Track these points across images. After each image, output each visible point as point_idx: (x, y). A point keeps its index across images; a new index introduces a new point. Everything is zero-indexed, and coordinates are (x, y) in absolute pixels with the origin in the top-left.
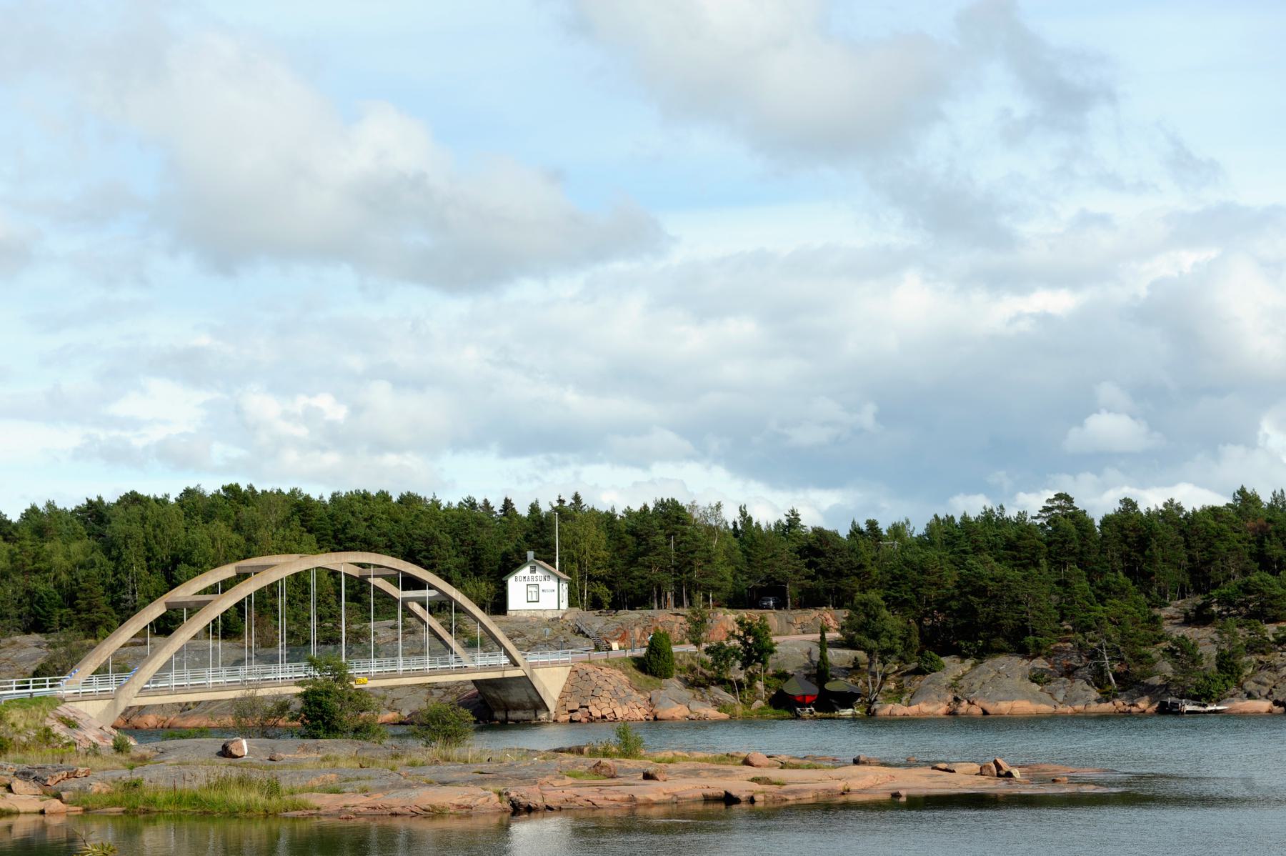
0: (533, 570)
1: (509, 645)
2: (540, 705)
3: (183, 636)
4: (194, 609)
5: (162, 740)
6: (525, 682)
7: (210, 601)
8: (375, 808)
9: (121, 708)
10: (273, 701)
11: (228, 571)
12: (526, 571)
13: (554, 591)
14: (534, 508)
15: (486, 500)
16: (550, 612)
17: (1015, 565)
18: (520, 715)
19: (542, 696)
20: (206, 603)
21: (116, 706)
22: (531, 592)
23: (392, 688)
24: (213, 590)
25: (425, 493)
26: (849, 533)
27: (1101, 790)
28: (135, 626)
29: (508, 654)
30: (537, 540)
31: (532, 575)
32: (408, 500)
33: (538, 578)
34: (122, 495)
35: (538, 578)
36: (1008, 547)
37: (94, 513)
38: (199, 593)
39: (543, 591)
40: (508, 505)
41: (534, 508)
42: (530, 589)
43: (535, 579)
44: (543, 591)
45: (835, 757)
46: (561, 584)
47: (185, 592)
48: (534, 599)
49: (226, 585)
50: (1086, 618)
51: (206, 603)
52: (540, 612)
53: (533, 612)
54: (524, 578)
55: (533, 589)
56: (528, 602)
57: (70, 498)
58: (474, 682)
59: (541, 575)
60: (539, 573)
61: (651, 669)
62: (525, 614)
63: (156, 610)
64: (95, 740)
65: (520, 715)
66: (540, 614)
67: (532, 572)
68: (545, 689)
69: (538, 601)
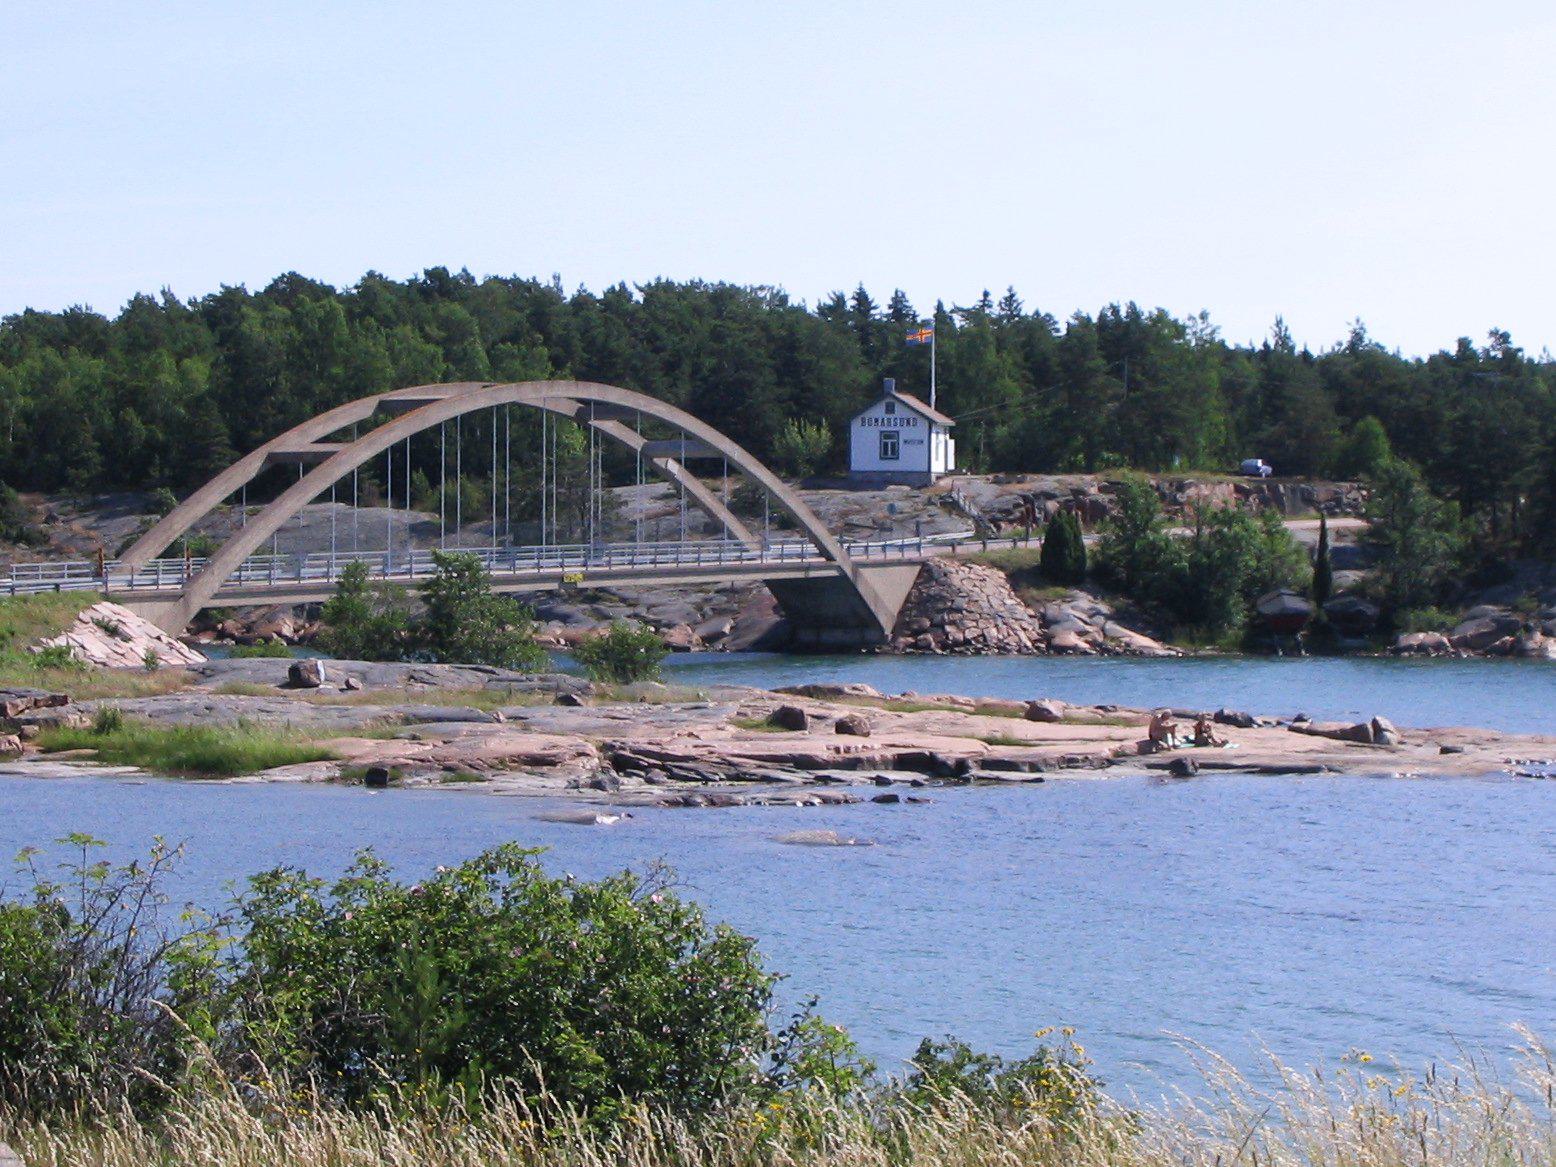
1: (818, 528)
2: (870, 620)
3: (293, 503)
4: (312, 462)
5: (225, 657)
6: (844, 586)
7: (334, 453)
8: (422, 761)
9: (195, 610)
11: (362, 409)
15: (464, 270)
18: (838, 636)
19: (872, 608)
20: (327, 455)
21: (187, 606)
23: (650, 589)
24: (343, 435)
25: (681, 278)
27: (996, 774)
28: (223, 488)
29: (815, 540)
31: (888, 416)
32: (661, 293)
36: (874, 342)
37: (226, 308)
38: (317, 442)
39: (905, 442)
40: (898, 303)
45: (563, 710)
46: (933, 436)
47: (296, 441)
49: (364, 428)
51: (327, 455)
54: (876, 420)
57: (194, 286)
58: (767, 583)
63: (251, 466)
65: (838, 636)
68: (876, 597)
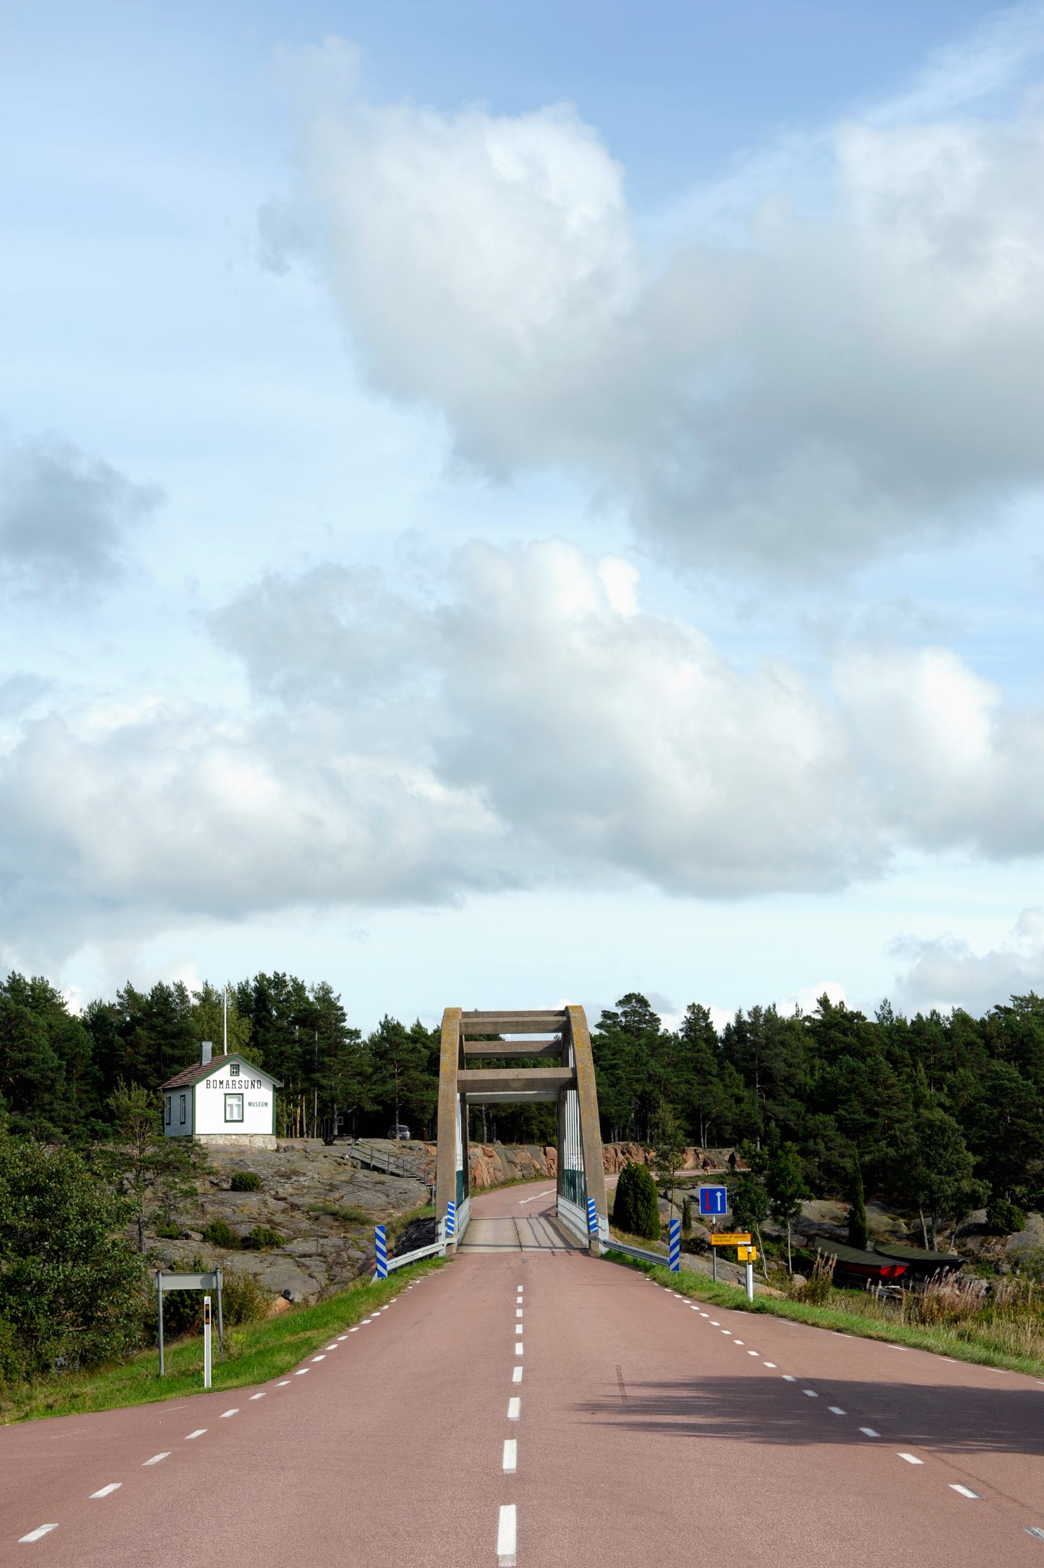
0: (235, 1070)
10: (199, 1261)
12: (224, 1073)
13: (266, 1104)
14: (698, 1018)
16: (260, 1138)
17: (415, 1080)
22: (231, 1106)
26: (733, 1024)
30: (161, 1026)
31: (234, 1078)
33: (243, 1084)
34: (713, 1025)
35: (243, 1084)
39: (250, 1104)
41: (698, 1018)
42: (229, 1101)
43: (237, 1085)
44: (250, 1104)
48: (236, 1118)
50: (967, 1293)
52: (244, 1137)
53: (234, 1137)
54: (221, 1083)
55: (233, 1101)
56: (226, 1121)
59: (247, 1078)
60: (243, 1076)
61: (637, 1225)
62: (221, 1141)
64: (161, 1289)
66: (245, 1141)
67: (232, 1074)
69: (242, 1121)
